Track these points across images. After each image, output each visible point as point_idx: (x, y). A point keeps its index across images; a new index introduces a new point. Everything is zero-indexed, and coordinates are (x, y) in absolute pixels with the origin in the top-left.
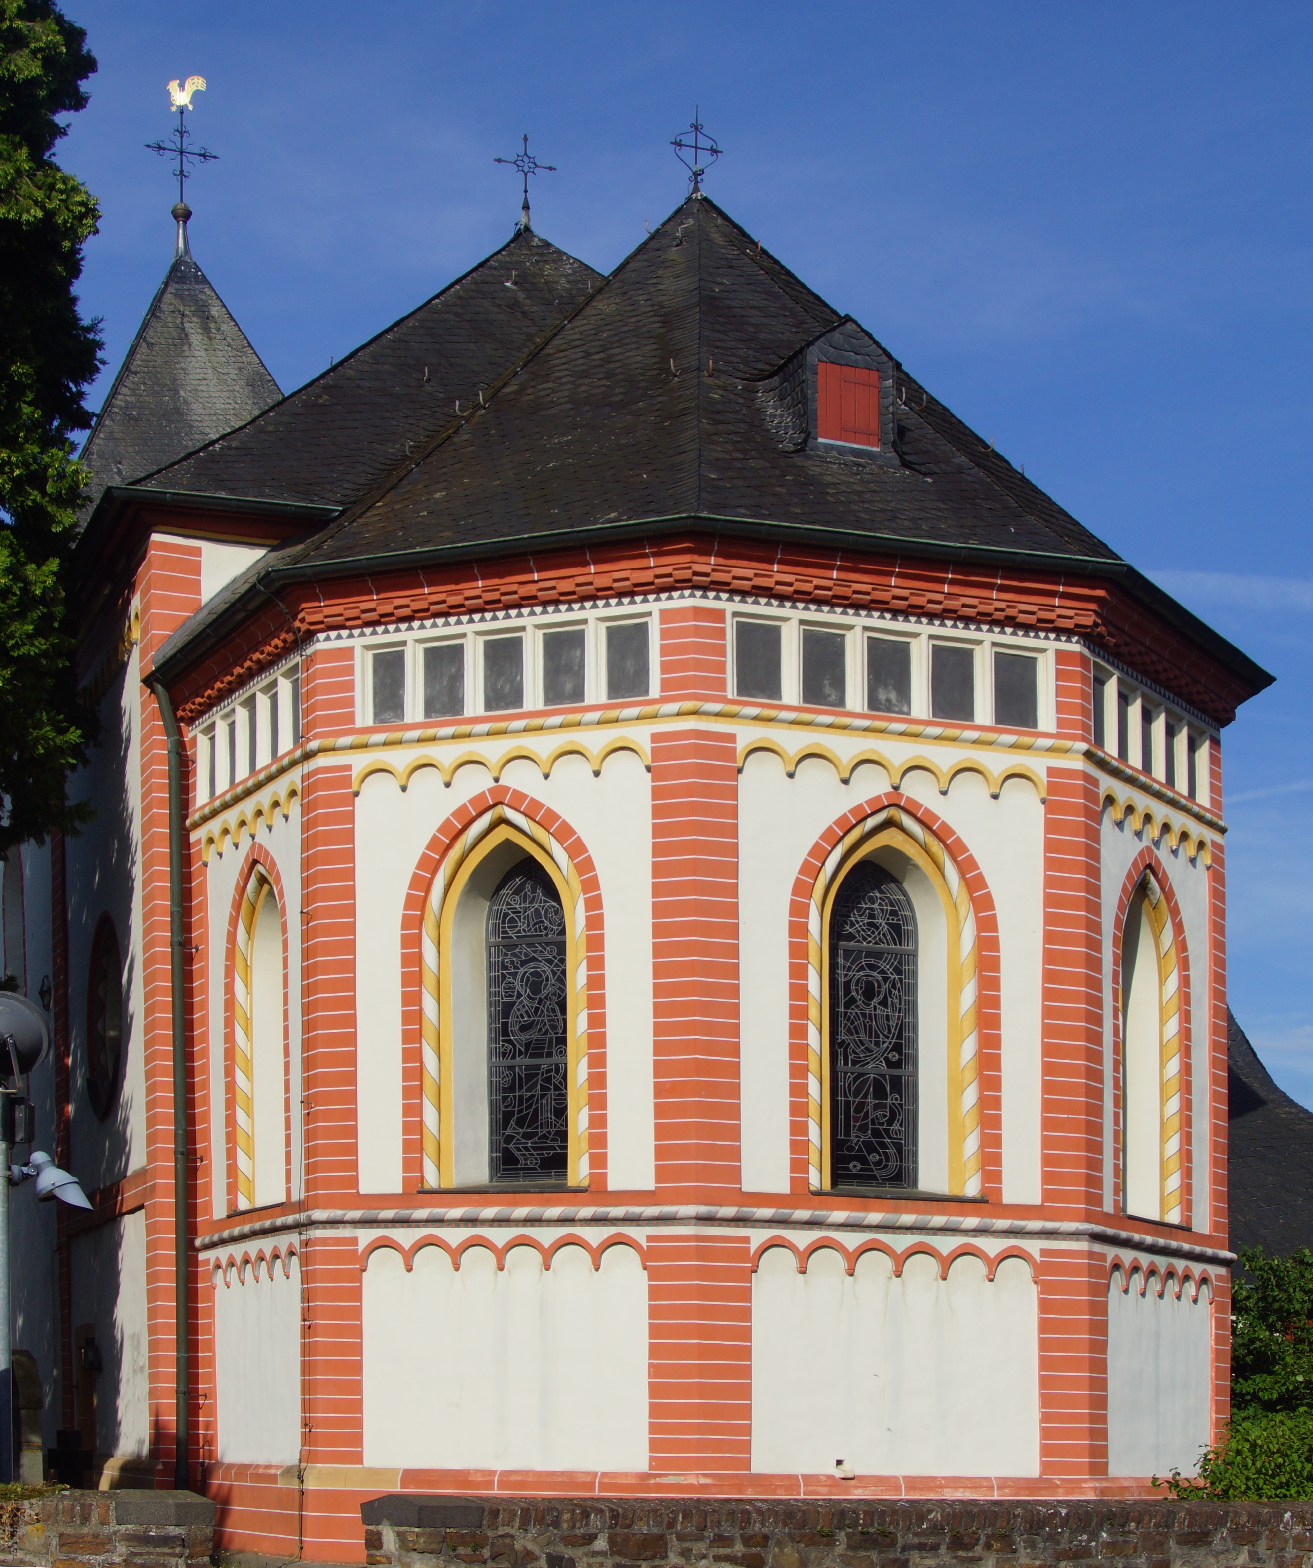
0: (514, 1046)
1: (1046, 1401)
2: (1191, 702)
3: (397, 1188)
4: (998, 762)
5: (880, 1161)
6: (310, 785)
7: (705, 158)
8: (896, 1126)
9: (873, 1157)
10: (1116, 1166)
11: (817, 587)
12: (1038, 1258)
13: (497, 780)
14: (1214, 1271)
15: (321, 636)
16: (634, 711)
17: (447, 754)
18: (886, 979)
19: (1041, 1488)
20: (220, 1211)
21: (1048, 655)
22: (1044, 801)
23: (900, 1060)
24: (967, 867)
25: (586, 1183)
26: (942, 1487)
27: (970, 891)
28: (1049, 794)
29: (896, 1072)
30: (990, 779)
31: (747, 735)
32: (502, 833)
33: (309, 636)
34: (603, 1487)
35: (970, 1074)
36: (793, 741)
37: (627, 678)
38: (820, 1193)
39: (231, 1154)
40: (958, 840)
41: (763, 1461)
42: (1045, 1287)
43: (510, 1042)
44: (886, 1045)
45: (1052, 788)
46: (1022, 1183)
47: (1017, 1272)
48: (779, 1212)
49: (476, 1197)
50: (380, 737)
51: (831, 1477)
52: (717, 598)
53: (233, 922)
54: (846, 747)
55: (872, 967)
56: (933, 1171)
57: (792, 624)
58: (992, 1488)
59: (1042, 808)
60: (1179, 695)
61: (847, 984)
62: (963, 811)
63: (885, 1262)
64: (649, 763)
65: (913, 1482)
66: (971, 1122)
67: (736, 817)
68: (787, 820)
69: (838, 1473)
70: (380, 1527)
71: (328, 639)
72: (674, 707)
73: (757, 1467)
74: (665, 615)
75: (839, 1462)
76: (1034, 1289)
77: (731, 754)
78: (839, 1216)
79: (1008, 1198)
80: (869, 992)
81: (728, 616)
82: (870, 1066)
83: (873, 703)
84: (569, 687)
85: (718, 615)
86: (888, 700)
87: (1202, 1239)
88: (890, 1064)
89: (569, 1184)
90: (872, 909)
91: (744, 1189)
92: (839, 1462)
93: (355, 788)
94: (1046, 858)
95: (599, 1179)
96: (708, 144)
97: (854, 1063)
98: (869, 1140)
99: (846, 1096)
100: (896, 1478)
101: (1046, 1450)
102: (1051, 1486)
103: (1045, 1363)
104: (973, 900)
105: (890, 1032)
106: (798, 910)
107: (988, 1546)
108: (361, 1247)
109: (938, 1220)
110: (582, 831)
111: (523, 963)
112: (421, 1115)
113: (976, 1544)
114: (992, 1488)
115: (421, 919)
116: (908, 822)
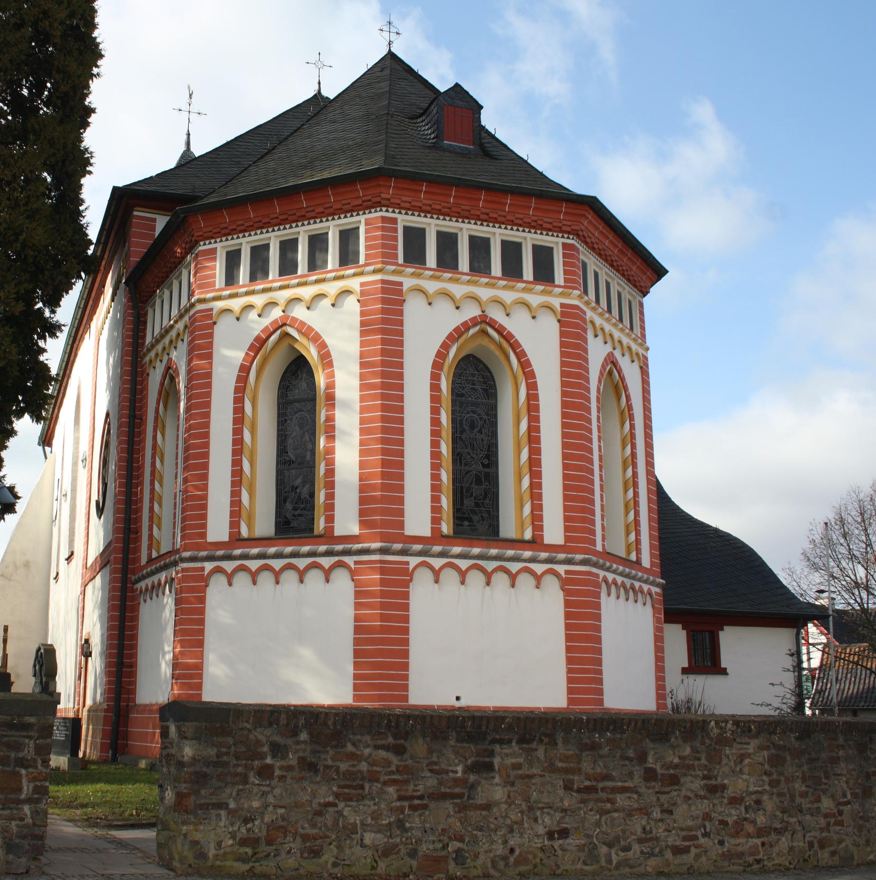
1: (569, 661)
2: (629, 280)
3: (226, 538)
4: (535, 300)
6: (193, 320)
7: (393, 37)
8: (487, 501)
12: (564, 576)
14: (655, 590)
15: (202, 243)
16: (351, 271)
17: (259, 300)
18: (481, 419)
20: (144, 560)
21: (555, 242)
22: (559, 321)
24: (521, 355)
25: (322, 532)
27: (523, 369)
29: (487, 470)
31: (408, 283)
32: (485, 342)
33: (196, 243)
35: (526, 470)
36: (432, 287)
37: (347, 257)
38: (447, 537)
39: (151, 529)
40: (516, 341)
42: (567, 592)
45: (563, 314)
46: (554, 532)
47: (552, 585)
48: (426, 545)
49: (265, 542)
50: (226, 293)
52: (393, 212)
53: (158, 403)
54: (458, 290)
55: (474, 412)
56: (508, 527)
57: (432, 227)
59: (558, 324)
60: (623, 275)
61: (461, 421)
62: (518, 325)
66: (527, 497)
67: (402, 326)
68: (429, 326)
70: (168, 723)
71: (205, 244)
72: (371, 268)
74: (563, 244)
75: (458, 698)
76: (561, 594)
77: (400, 292)
78: (457, 550)
79: (547, 541)
80: (472, 426)
81: (399, 221)
82: (474, 466)
83: (472, 268)
88: (484, 465)
92: (458, 698)
93: (214, 320)
94: (561, 351)
95: (330, 529)
96: (395, 30)
97: (466, 465)
98: (474, 507)
101: (570, 691)
104: (524, 373)
106: (435, 377)
107: (541, 741)
108: (411, 567)
109: (510, 553)
111: (296, 413)
112: (240, 497)
113: (534, 740)
115: (245, 388)
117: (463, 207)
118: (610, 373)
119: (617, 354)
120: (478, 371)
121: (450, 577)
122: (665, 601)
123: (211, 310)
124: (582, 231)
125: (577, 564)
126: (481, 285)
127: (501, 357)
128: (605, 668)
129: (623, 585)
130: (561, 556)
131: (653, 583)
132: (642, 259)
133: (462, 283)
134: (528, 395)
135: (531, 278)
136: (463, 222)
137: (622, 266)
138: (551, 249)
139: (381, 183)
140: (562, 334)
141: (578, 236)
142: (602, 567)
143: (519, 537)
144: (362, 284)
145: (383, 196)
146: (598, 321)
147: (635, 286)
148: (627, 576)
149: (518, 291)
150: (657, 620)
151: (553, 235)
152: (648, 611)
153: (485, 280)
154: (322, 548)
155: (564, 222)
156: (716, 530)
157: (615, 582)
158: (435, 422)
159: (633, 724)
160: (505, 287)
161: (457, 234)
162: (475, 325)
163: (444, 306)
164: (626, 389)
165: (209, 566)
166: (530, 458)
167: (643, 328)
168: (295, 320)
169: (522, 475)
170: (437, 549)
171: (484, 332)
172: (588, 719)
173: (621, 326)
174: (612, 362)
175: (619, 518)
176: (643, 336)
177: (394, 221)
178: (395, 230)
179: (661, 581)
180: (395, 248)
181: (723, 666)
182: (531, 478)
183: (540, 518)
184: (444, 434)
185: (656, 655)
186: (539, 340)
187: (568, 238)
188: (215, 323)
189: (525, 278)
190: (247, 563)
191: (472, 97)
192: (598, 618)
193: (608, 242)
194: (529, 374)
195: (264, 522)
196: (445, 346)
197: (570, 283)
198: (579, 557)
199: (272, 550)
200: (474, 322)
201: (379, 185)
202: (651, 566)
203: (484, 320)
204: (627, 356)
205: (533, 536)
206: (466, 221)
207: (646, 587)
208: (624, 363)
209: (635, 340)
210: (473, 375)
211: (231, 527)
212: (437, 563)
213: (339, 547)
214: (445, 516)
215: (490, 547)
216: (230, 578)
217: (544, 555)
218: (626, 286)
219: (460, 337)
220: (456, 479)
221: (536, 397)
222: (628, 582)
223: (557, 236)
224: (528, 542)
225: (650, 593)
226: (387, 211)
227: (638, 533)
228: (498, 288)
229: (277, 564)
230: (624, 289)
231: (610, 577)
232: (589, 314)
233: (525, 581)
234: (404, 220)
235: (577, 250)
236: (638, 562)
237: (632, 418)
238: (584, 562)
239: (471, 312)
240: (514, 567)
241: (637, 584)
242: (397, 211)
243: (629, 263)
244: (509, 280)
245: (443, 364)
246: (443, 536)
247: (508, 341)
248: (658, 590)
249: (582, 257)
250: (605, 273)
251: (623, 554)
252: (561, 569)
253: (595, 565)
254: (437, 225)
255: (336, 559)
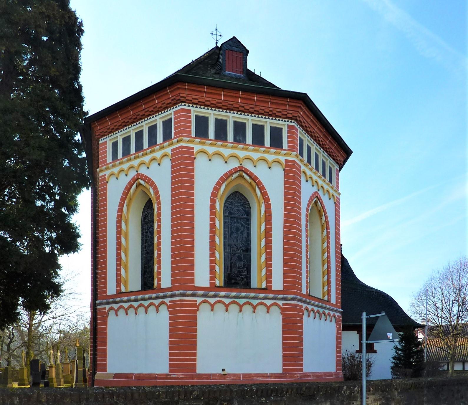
0: (147, 251)
1: (284, 350)
4: (270, 157)
5: (240, 280)
8: (245, 269)
9: (238, 278)
10: (307, 281)
11: (217, 103)
12: (282, 306)
13: (137, 171)
14: (337, 314)
18: (242, 226)
19: (282, 377)
21: (284, 124)
22: (284, 170)
23: (246, 250)
24: (262, 189)
26: (253, 377)
28: (285, 168)
29: (245, 253)
30: (269, 162)
31: (197, 148)
32: (242, 182)
34: (158, 378)
35: (263, 251)
36: (211, 150)
41: (201, 369)
42: (284, 315)
43: (146, 250)
44: (242, 245)
46: (278, 284)
47: (164, 310)
51: (220, 374)
52: (189, 106)
54: (226, 152)
55: (238, 222)
57: (212, 115)
58: (240, 378)
60: (326, 151)
62: (261, 172)
63: (237, 308)
64: (284, 168)
65: (246, 376)
66: (263, 265)
68: (210, 171)
69: (223, 373)
73: (198, 372)
74: (289, 127)
75: (224, 370)
76: (281, 316)
77: (193, 153)
79: (274, 288)
83: (235, 140)
84: (154, 141)
85: (189, 111)
86: (240, 139)
87: (333, 305)
89: (196, 285)
90: (238, 206)
91: (195, 286)
95: (159, 285)
99: (230, 260)
100: (240, 374)
102: (286, 376)
103: (284, 338)
104: (264, 199)
105: (243, 241)
106: (213, 201)
108: (198, 303)
110: (156, 183)
114: (240, 378)
116: (245, 175)
117: (229, 102)
118: (316, 203)
119: (321, 193)
120: (241, 200)
121: (220, 308)
122: (343, 321)
123: (105, 175)
124: (299, 117)
125: (289, 300)
126: (239, 149)
127: (251, 191)
128: (304, 353)
129: (318, 312)
130: (281, 296)
131: (336, 311)
132: (338, 143)
133: (229, 148)
134: (266, 211)
135: (269, 145)
136: (230, 112)
137: (325, 145)
138: (281, 129)
139: (179, 86)
140: (286, 177)
141: (296, 120)
142: (305, 302)
143: (259, 287)
144: (173, 150)
145: (182, 95)
146: (309, 173)
147: (334, 159)
148: (321, 307)
149: (260, 152)
150: (338, 329)
151: (282, 120)
152: (333, 324)
153: (241, 146)
154: (154, 295)
155: (288, 112)
156: (376, 290)
157: (313, 310)
158: (213, 225)
159: (290, 390)
160: (253, 150)
161: (226, 121)
162: (236, 172)
163: (218, 162)
164: (325, 212)
165: (108, 307)
166: (266, 245)
167: (338, 183)
168: (142, 175)
169: (262, 254)
170: (212, 293)
171: (241, 176)
172: (257, 390)
173: (331, 185)
174: (317, 197)
175: (318, 279)
176: (338, 187)
177: (189, 111)
178: (190, 117)
179: (341, 310)
180: (190, 127)
181: (375, 349)
182: (266, 255)
183: (270, 277)
184: (217, 232)
185: (337, 346)
186: (273, 180)
187: (291, 122)
188: (107, 182)
189: (266, 146)
190: (123, 304)
191: (242, 45)
192: (302, 328)
193: (316, 128)
194: (267, 200)
195: (134, 282)
196: (219, 184)
197: (291, 148)
198: (290, 296)
199: (140, 297)
200: (236, 170)
201: (179, 88)
202: (336, 303)
203: (241, 169)
204: (327, 195)
205: (267, 286)
206: (232, 112)
207: (332, 313)
208: (325, 199)
209: (332, 188)
210: (238, 203)
211: (117, 287)
212: (212, 300)
213: (162, 294)
214: (217, 276)
215: (241, 292)
216: (116, 312)
217: (271, 296)
218: (328, 158)
219: (227, 179)
220: (227, 258)
221: (270, 212)
222: (321, 310)
223: (285, 121)
224: (263, 289)
225: (334, 316)
226: (185, 105)
227: (329, 286)
228: (249, 151)
229: (136, 304)
230: (327, 160)
231: (310, 307)
232: (303, 168)
233: (260, 308)
234: (196, 111)
235: (297, 130)
236: (329, 301)
237: (328, 228)
238: (293, 299)
239: (234, 164)
240: (255, 302)
241: (327, 312)
242: (191, 105)
243: (330, 144)
244: (255, 147)
245: (217, 194)
246: (216, 287)
247: (255, 181)
248: (339, 315)
249: (299, 135)
250: (315, 148)
251: (321, 298)
252: (281, 303)
253: (300, 300)
254: (214, 115)
255: (161, 300)
